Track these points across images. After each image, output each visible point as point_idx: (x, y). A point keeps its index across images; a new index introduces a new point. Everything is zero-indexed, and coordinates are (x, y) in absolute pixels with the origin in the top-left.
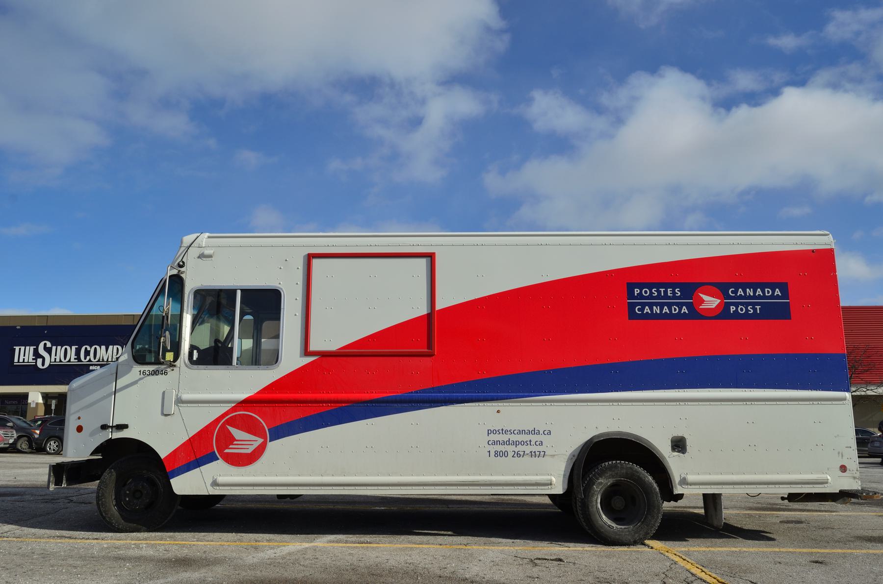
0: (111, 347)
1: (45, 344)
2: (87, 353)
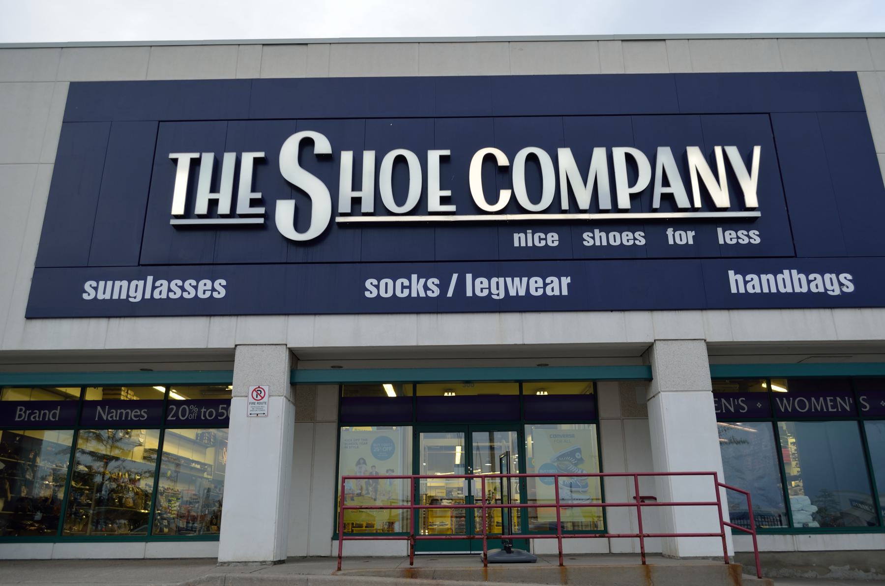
0: (599, 155)
1: (489, 159)
2: (497, 177)
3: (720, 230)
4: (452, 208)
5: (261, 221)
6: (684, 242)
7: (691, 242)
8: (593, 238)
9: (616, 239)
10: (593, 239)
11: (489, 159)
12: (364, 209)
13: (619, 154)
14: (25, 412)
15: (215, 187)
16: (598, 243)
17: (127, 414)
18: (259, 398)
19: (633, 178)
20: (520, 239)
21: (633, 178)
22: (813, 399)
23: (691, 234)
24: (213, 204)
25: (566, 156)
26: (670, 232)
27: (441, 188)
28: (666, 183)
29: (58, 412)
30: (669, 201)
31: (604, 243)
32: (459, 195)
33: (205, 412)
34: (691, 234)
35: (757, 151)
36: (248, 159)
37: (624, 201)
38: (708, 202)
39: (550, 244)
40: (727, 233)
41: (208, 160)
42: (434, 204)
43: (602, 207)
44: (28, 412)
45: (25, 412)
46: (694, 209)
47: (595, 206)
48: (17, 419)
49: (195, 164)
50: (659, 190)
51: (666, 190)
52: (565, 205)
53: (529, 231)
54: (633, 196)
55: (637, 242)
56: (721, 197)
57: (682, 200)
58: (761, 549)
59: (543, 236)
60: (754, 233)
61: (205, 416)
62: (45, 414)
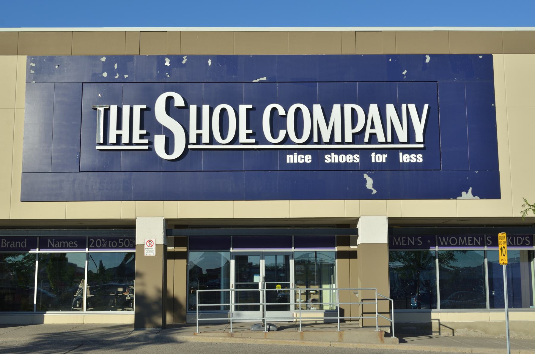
0: (336, 108)
1: (274, 111)
3: (401, 154)
4: (253, 141)
5: (146, 147)
6: (380, 161)
7: (384, 161)
8: (331, 158)
9: (345, 159)
11: (274, 111)
13: (348, 108)
14: (6, 243)
15: (119, 126)
16: (333, 161)
17: (66, 244)
18: (150, 246)
19: (354, 124)
20: (290, 159)
21: (354, 124)
22: (460, 238)
23: (385, 156)
24: (119, 137)
25: (317, 108)
26: (373, 155)
28: (373, 127)
29: (25, 243)
30: (373, 137)
32: (257, 134)
33: (111, 243)
34: (385, 156)
35: (426, 106)
36: (137, 109)
37: (349, 138)
38: (395, 139)
39: (307, 161)
40: (405, 155)
41: (114, 109)
42: (242, 138)
45: (6, 243)
46: (386, 143)
47: (332, 140)
48: (2, 247)
49: (107, 112)
50: (368, 131)
51: (373, 131)
52: (316, 140)
53: (295, 154)
54: (353, 134)
56: (403, 136)
57: (381, 138)
59: (303, 156)
61: (111, 245)
62: (18, 244)
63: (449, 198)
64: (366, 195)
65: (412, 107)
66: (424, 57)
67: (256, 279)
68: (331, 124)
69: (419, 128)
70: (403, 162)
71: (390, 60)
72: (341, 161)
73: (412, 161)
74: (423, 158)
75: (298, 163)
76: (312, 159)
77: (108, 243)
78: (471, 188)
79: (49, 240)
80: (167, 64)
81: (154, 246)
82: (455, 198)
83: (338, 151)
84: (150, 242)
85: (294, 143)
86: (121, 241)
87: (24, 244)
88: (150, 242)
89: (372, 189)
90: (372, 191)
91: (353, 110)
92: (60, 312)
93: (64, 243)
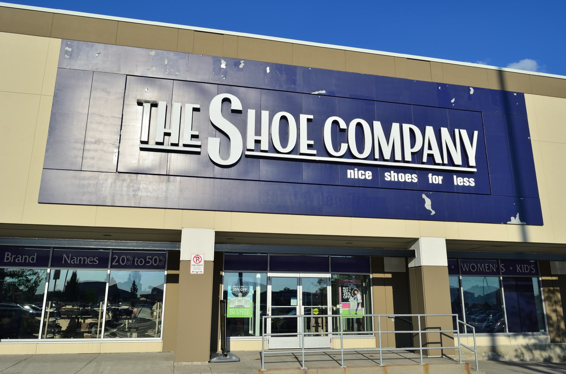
0: (395, 127)
1: (335, 123)
2: (339, 135)
3: (455, 177)
4: (314, 152)
7: (441, 183)
8: (390, 176)
10: (391, 176)
11: (335, 123)
12: (263, 148)
13: (406, 127)
14: (11, 257)
16: (393, 180)
17: (84, 260)
18: (198, 262)
20: (352, 174)
21: (413, 145)
24: (258, 142)
26: (430, 175)
27: (308, 139)
28: (430, 148)
29: (35, 257)
31: (396, 180)
33: (137, 261)
34: (441, 178)
35: (476, 133)
37: (408, 157)
38: (451, 162)
40: (459, 178)
42: (303, 149)
43: (471, 164)
44: (13, 256)
45: (11, 257)
46: (443, 164)
47: (393, 159)
48: (5, 261)
50: (426, 151)
51: (430, 152)
52: (377, 156)
53: (356, 169)
55: (413, 180)
56: (457, 159)
57: (438, 160)
58: (478, 344)
59: (363, 172)
60: (472, 180)
61: (137, 263)
63: (500, 223)
64: (424, 216)
65: (464, 133)
66: (468, 89)
67: (293, 302)
68: (392, 142)
69: (472, 152)
70: (458, 185)
71: (440, 88)
72: (400, 180)
73: (465, 184)
74: (475, 182)
75: (359, 179)
76: (373, 176)
77: (134, 261)
78: (518, 214)
79: (65, 255)
80: (223, 66)
81: (202, 263)
82: (505, 223)
83: (398, 170)
84: (197, 257)
85: (355, 158)
86: (149, 258)
87: (33, 259)
88: (197, 257)
89: (431, 210)
90: (431, 212)
91: (411, 130)
92: (72, 339)
93: (82, 259)
